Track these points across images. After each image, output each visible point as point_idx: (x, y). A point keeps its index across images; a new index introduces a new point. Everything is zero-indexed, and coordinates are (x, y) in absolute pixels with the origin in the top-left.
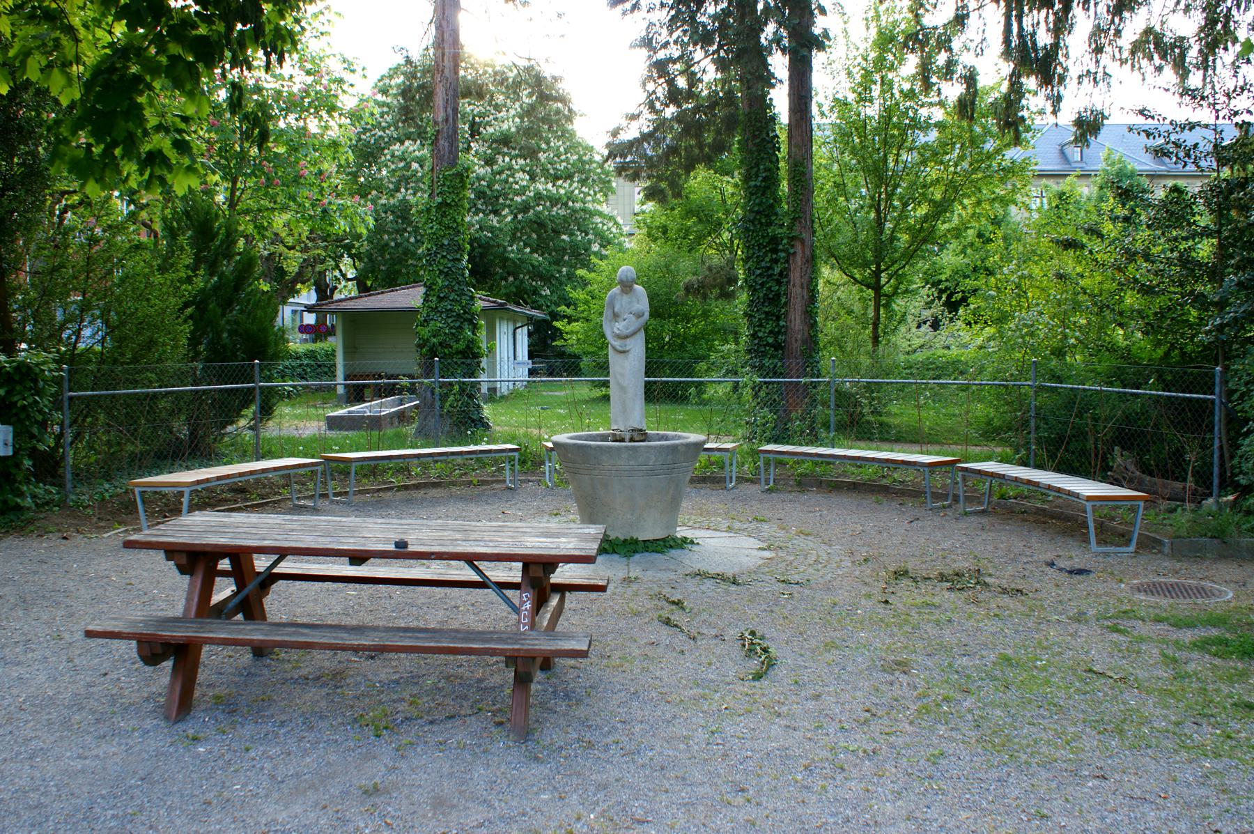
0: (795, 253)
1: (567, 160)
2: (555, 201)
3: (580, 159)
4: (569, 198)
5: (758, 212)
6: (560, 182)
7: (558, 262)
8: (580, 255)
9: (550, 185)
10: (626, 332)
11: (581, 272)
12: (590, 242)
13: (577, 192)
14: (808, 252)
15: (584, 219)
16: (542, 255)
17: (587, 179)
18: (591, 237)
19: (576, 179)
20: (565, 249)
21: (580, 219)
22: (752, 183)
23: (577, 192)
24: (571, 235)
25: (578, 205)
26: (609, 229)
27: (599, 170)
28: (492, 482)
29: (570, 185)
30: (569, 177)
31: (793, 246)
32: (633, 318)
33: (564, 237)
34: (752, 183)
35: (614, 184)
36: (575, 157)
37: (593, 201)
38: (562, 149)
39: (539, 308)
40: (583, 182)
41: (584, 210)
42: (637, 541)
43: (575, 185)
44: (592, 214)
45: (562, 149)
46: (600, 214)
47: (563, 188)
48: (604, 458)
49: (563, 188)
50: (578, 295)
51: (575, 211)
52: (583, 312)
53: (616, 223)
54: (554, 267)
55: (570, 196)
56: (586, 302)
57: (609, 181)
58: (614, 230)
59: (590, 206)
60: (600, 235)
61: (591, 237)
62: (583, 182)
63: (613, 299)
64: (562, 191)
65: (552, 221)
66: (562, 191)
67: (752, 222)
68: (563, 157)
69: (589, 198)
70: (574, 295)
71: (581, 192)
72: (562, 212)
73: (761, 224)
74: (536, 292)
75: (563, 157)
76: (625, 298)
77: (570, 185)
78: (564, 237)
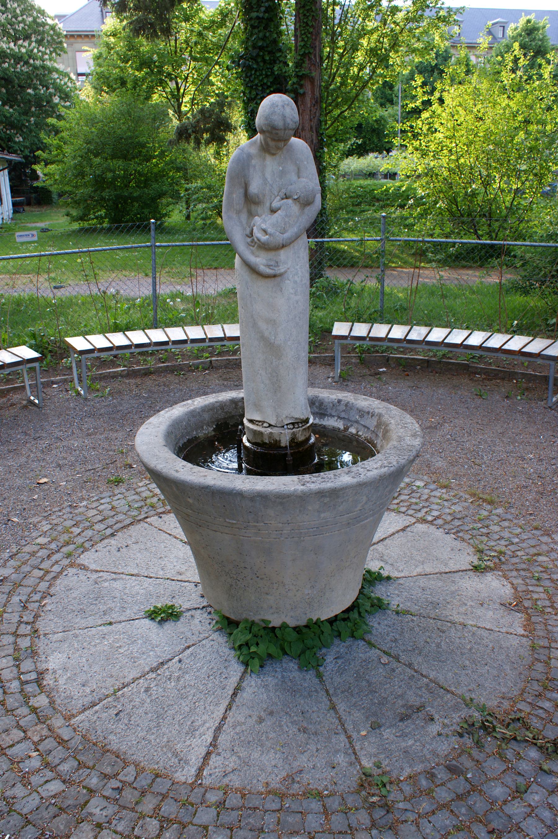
0: (304, 94)
1: (23, 21)
2: (18, 59)
3: (35, 21)
4: (30, 57)
5: (261, 48)
6: (20, 42)
7: (26, 113)
8: (45, 107)
9: (12, 45)
10: (280, 238)
11: (50, 120)
12: (51, 95)
13: (36, 51)
14: (317, 94)
15: (44, 75)
16: (11, 107)
17: (43, 39)
18: (51, 90)
19: (33, 39)
20: (30, 101)
21: (42, 75)
22: (254, 15)
23: (36, 51)
24: (35, 89)
25: (38, 63)
26: (65, 84)
27: (52, 32)
28: (9, 390)
29: (30, 45)
30: (27, 37)
31: (302, 86)
32: (295, 208)
33: (30, 91)
34: (254, 15)
35: (65, 45)
36: (31, 19)
37: (50, 60)
38: (18, 11)
39: (15, 152)
40: (40, 42)
41: (44, 67)
42: (318, 623)
43: (34, 44)
44: (51, 70)
45: (18, 11)
46: (57, 71)
47: (23, 47)
48: (271, 512)
49: (23, 47)
50: (51, 140)
51: (36, 68)
52: (57, 156)
53: (70, 79)
54: (23, 117)
55: (30, 54)
56: (59, 147)
57: (61, 43)
58: (69, 84)
59: (48, 63)
60: (59, 89)
61: (51, 90)
62: (40, 42)
63: (243, 167)
64: (23, 50)
65: (18, 78)
66: (23, 50)
67: (254, 59)
68: (20, 19)
69: (46, 57)
70: (47, 140)
71: (39, 51)
72: (25, 69)
73: (264, 61)
74: (10, 139)
75: (20, 19)
76: (271, 165)
77: (30, 45)
78: (30, 91)
